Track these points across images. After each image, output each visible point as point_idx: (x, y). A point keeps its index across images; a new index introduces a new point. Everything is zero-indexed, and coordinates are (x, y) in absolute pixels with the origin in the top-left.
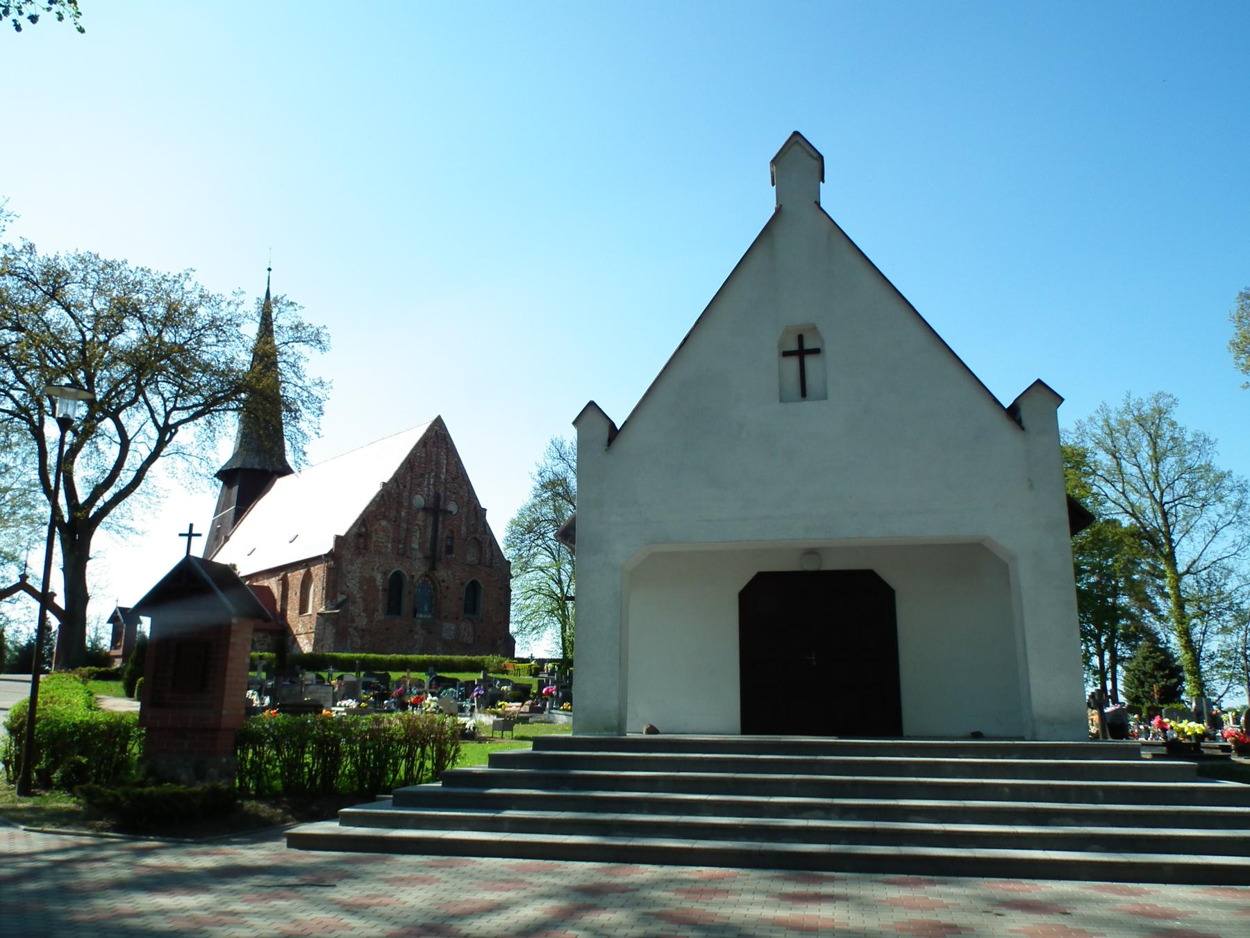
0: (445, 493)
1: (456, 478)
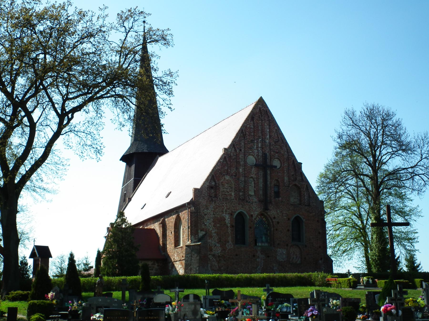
0: (270, 153)
1: (277, 142)
